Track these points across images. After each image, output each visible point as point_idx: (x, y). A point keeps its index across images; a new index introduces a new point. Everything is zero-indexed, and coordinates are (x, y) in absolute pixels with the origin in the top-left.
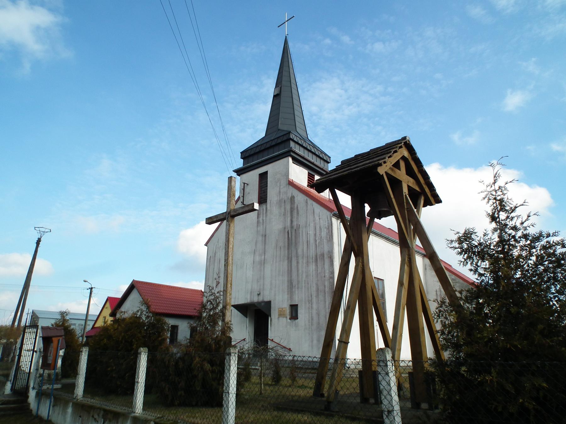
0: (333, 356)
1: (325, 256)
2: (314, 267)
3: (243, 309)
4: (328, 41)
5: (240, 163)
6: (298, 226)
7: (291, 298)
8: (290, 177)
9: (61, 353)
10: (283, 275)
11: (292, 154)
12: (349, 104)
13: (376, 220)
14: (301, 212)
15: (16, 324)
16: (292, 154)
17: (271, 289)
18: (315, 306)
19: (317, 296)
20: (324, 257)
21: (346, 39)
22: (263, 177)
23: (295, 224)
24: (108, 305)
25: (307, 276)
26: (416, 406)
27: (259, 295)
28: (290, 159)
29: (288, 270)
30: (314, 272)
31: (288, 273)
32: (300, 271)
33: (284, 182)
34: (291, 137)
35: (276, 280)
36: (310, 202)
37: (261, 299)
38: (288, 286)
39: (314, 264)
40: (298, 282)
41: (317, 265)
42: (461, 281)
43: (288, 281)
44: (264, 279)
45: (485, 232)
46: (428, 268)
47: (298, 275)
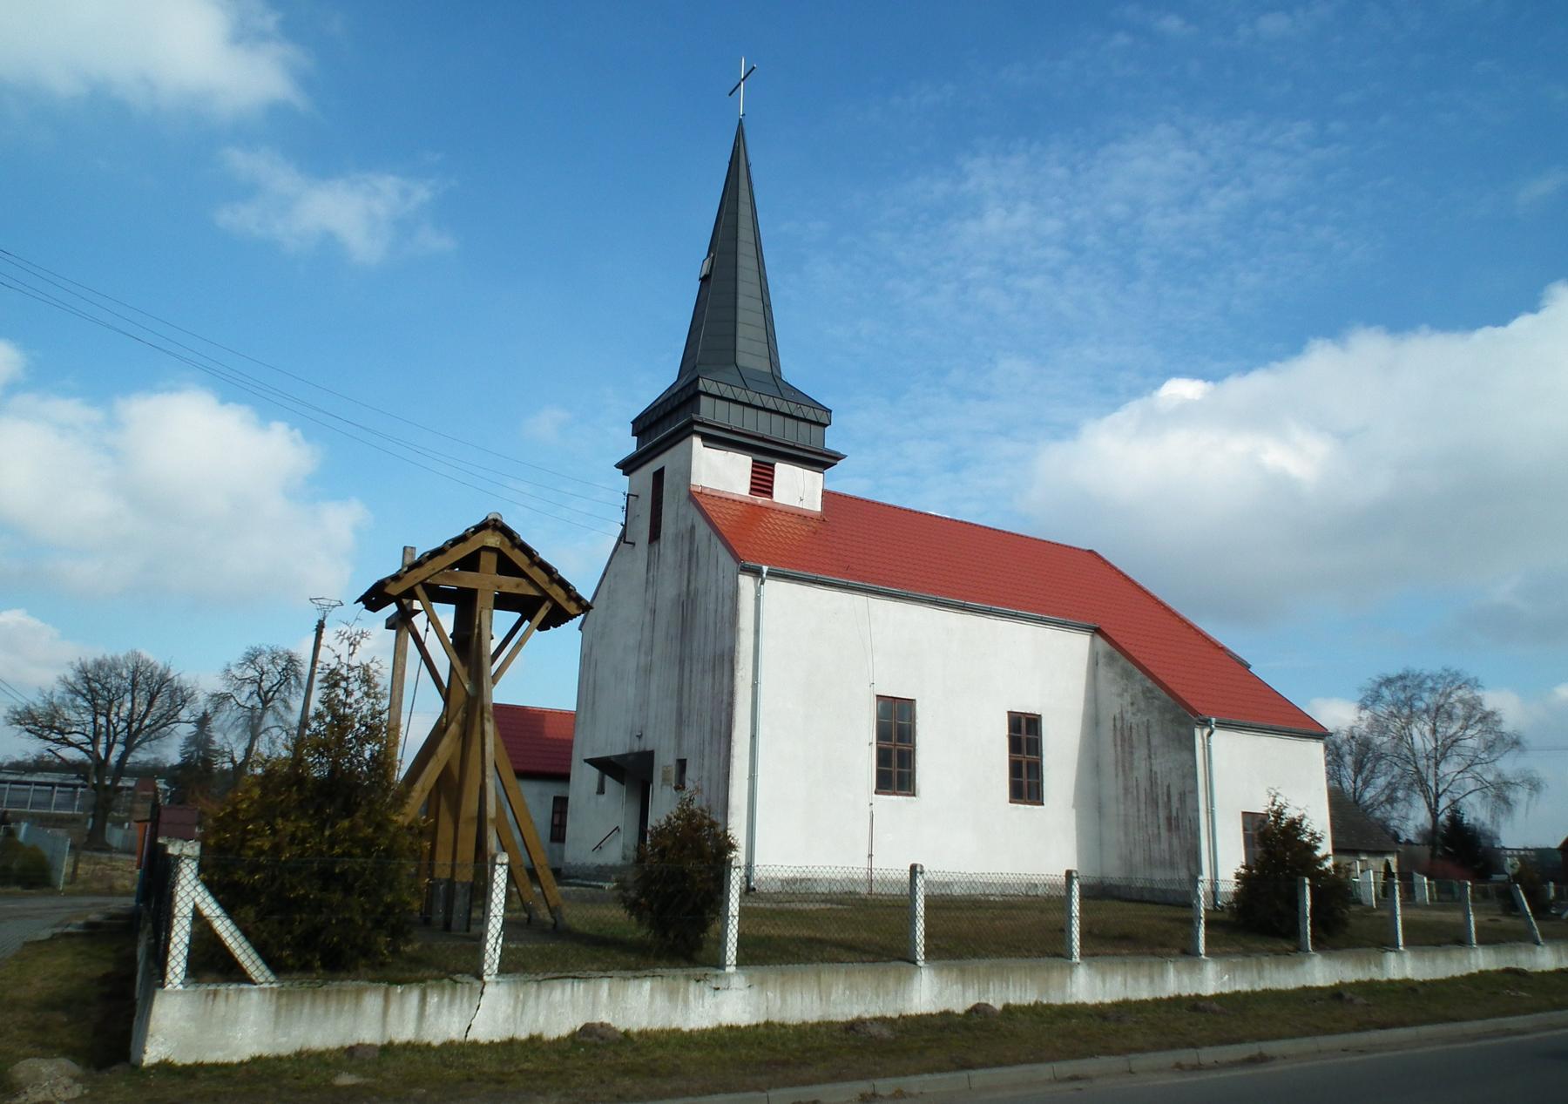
3: (607, 766)
4: (1122, 39)
5: (630, 446)
6: (697, 590)
7: (679, 745)
8: (693, 481)
11: (696, 428)
12: (1219, 185)
14: (702, 561)
16: (696, 428)
18: (706, 763)
19: (711, 744)
21: (1172, 24)
22: (659, 476)
23: (692, 587)
24: (1103, 671)
27: (640, 737)
28: (697, 442)
33: (684, 493)
34: (701, 387)
36: (714, 539)
42: (1164, 695)
46: (1102, 661)
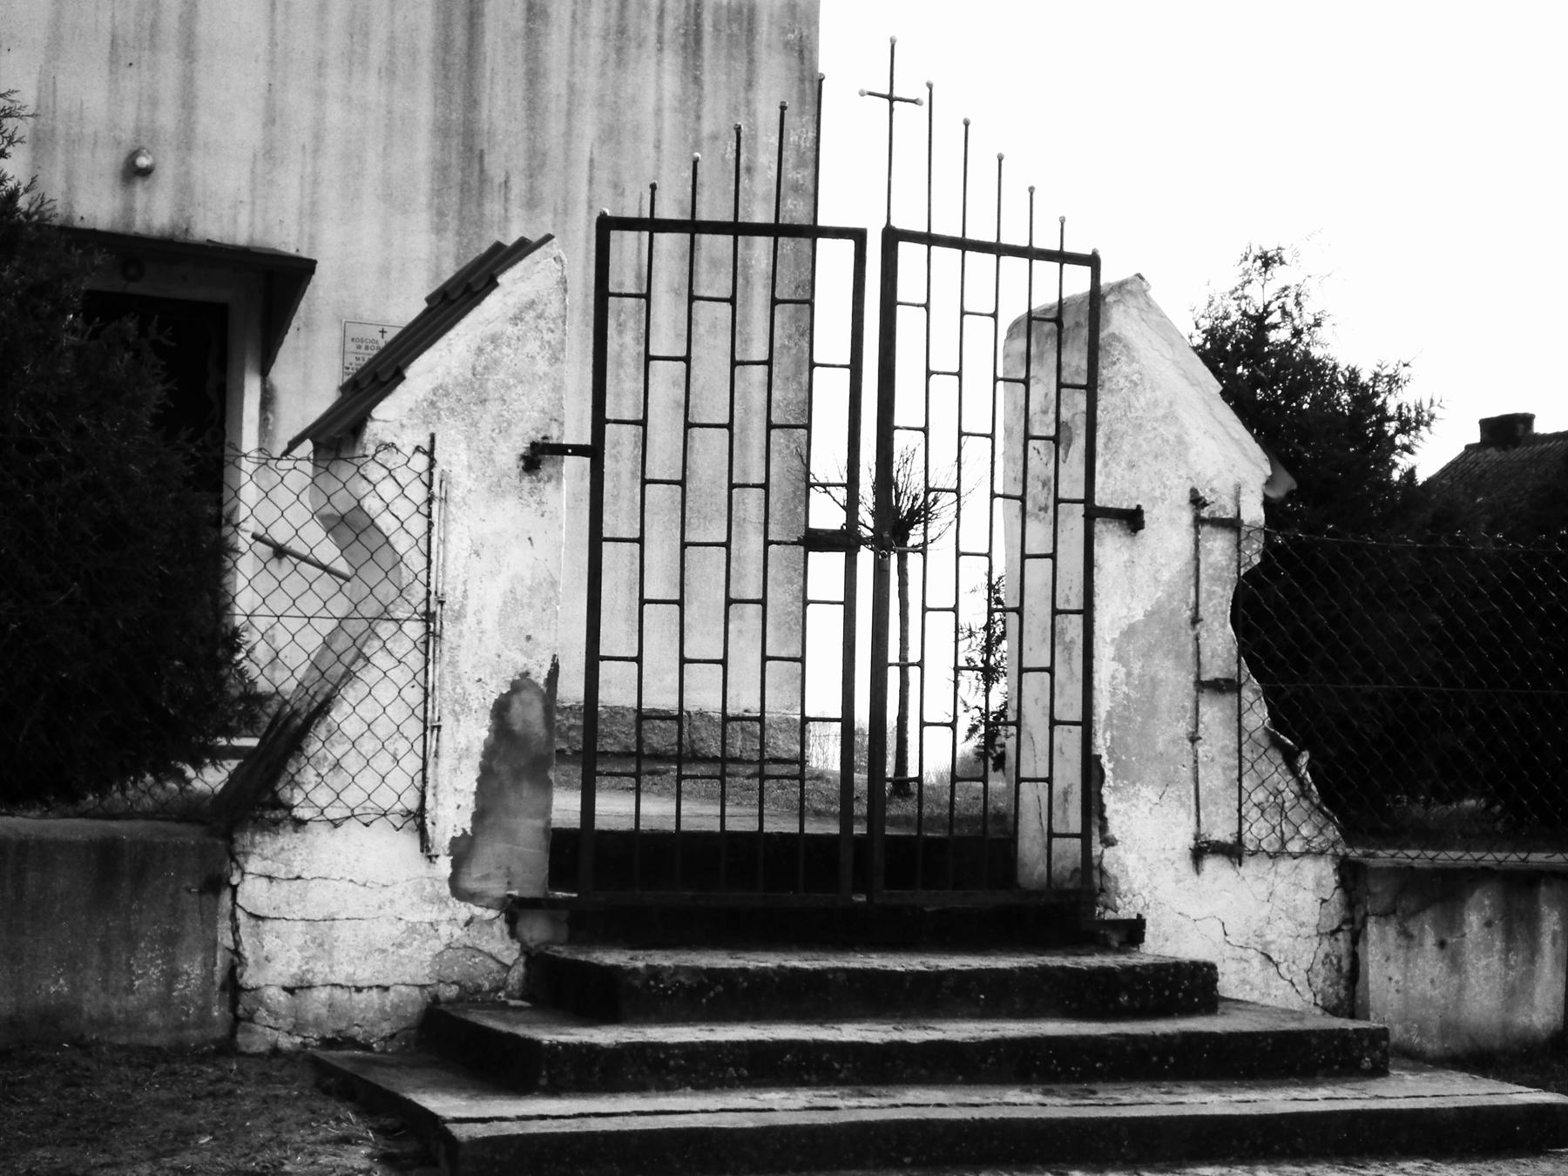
0: (890, 770)
1: (764, 30)
2: (671, 83)
9: (223, 742)
10: (390, 72)
13: (914, 834)
15: (861, 778)
17: (270, 154)
20: (751, 32)
25: (611, 134)
26: (99, 277)
29: (444, 44)
30: (670, 121)
31: (443, 66)
32: (555, 85)
35: (320, 95)
37: (155, 212)
38: (441, 171)
39: (671, 60)
40: (536, 162)
41: (693, 76)
43: (442, 131)
44: (189, 53)
45: (1378, 370)
47: (534, 107)
